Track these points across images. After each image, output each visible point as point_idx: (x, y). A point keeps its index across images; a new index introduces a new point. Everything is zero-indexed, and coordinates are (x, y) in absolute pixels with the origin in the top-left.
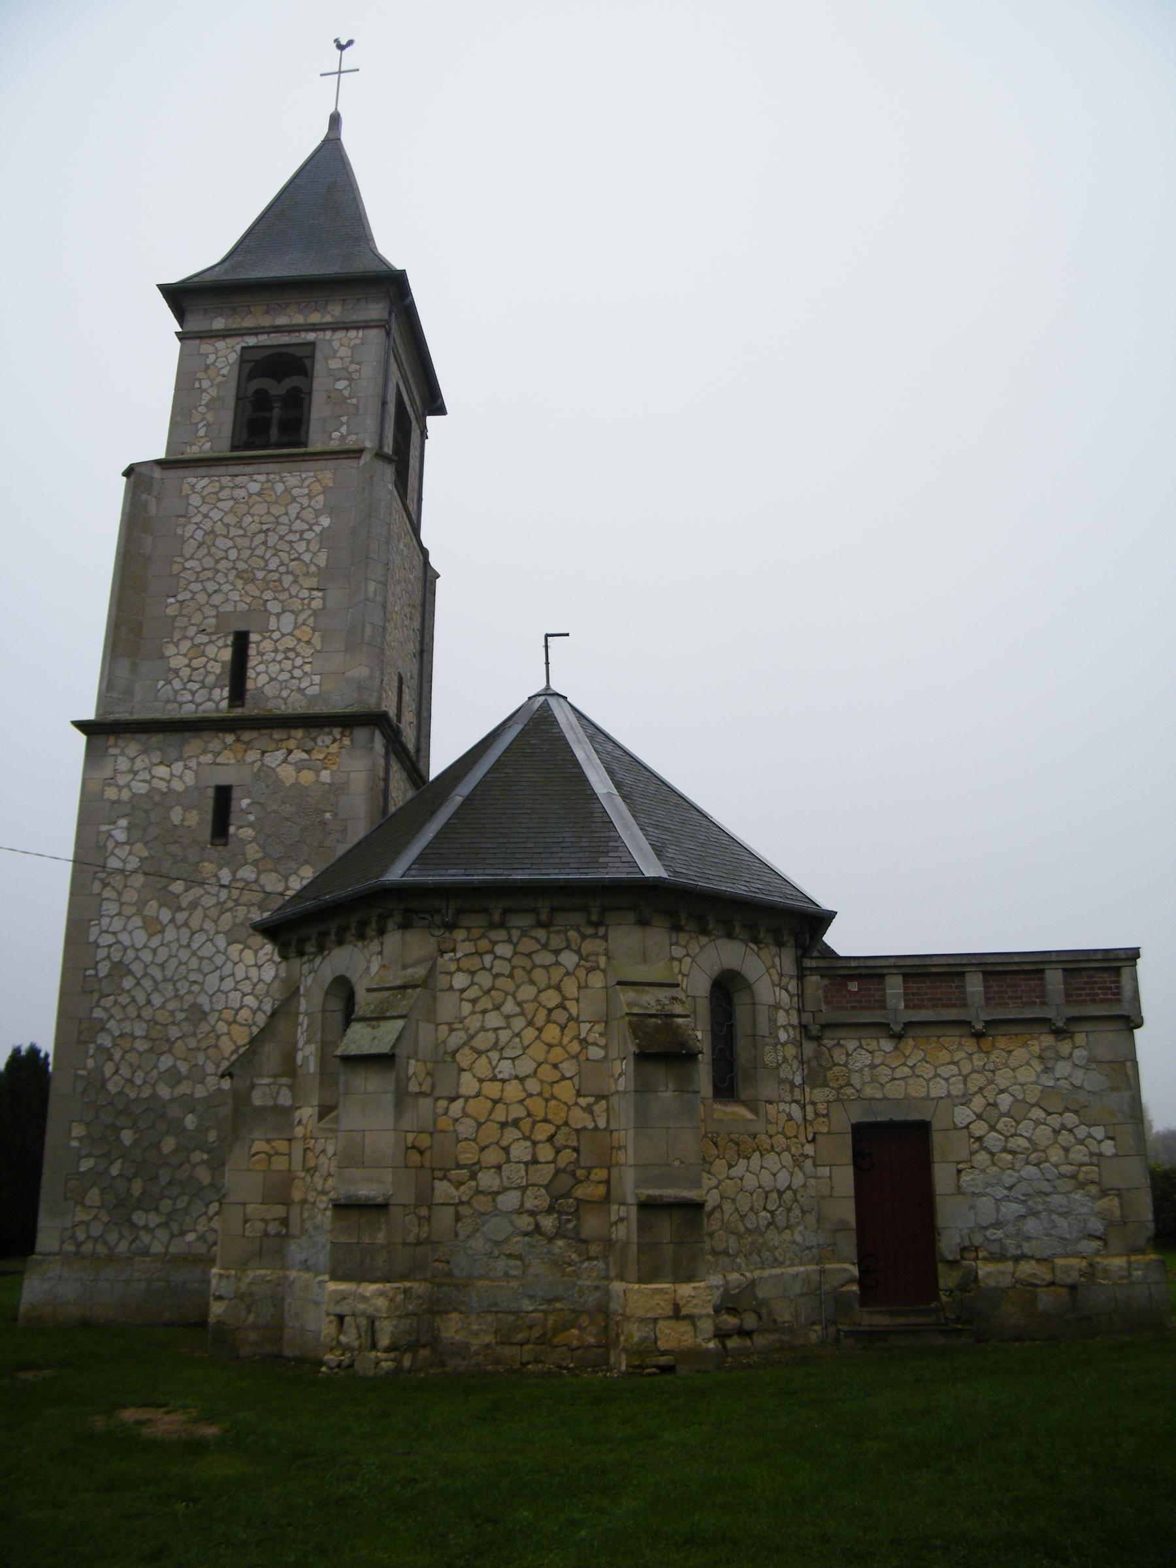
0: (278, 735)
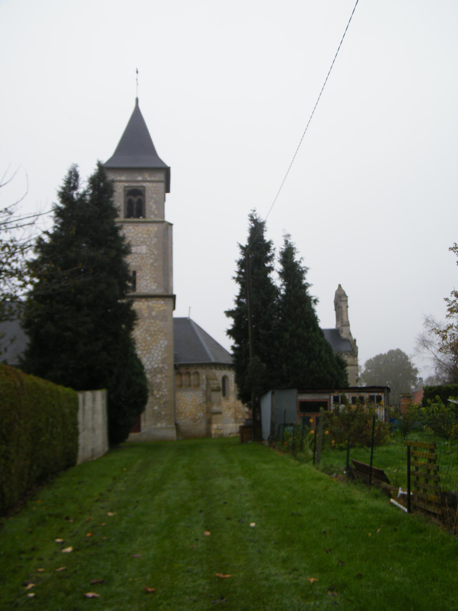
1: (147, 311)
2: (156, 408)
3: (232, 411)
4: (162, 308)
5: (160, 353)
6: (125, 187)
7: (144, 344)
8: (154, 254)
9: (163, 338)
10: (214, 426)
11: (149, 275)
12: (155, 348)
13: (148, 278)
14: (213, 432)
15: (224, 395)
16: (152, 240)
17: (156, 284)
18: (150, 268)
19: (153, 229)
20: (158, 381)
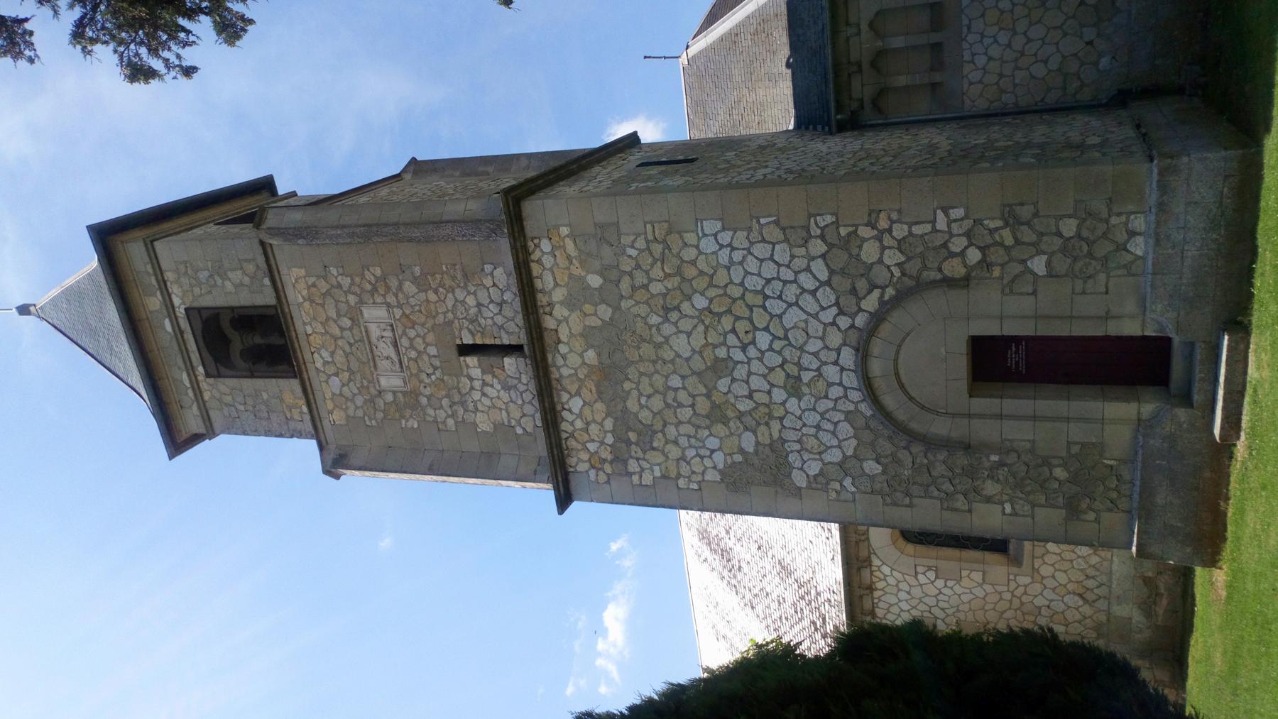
0: (542, 299)
1: (588, 308)
2: (1038, 265)
5: (761, 250)
6: (208, 375)
7: (727, 322)
8: (384, 278)
11: (460, 294)
13: (471, 301)
16: (340, 286)
17: (488, 268)
18: (436, 292)
19: (302, 285)
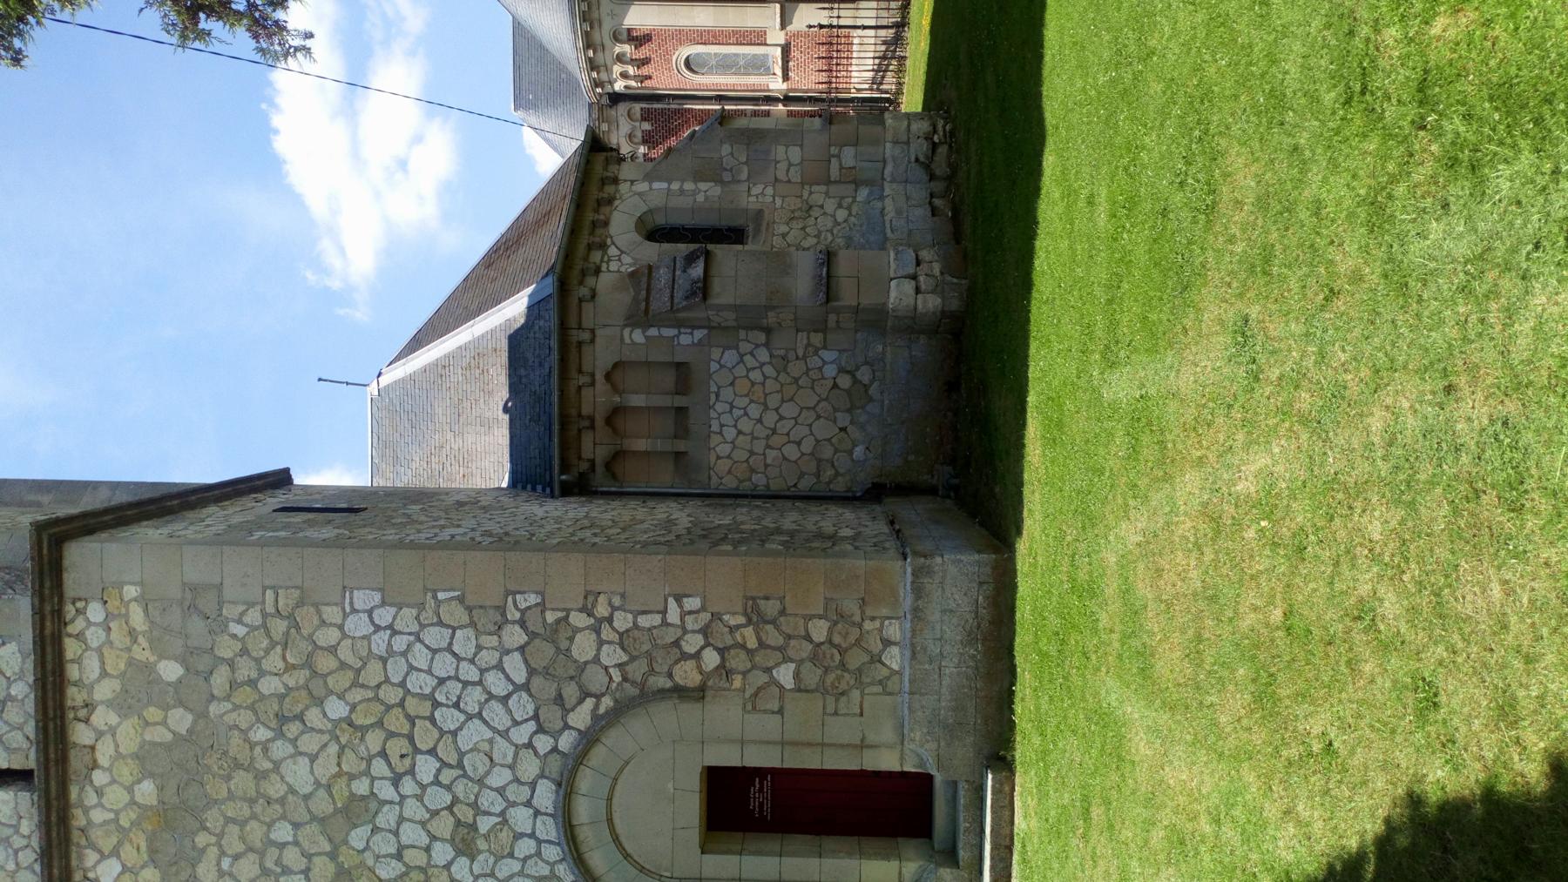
1: (153, 713)
3: (817, 195)
4: (137, 616)
5: (435, 636)
7: (374, 741)
9: (332, 613)
10: (899, 295)
12: (396, 670)
14: (931, 303)
15: (734, 235)
20: (612, 656)
